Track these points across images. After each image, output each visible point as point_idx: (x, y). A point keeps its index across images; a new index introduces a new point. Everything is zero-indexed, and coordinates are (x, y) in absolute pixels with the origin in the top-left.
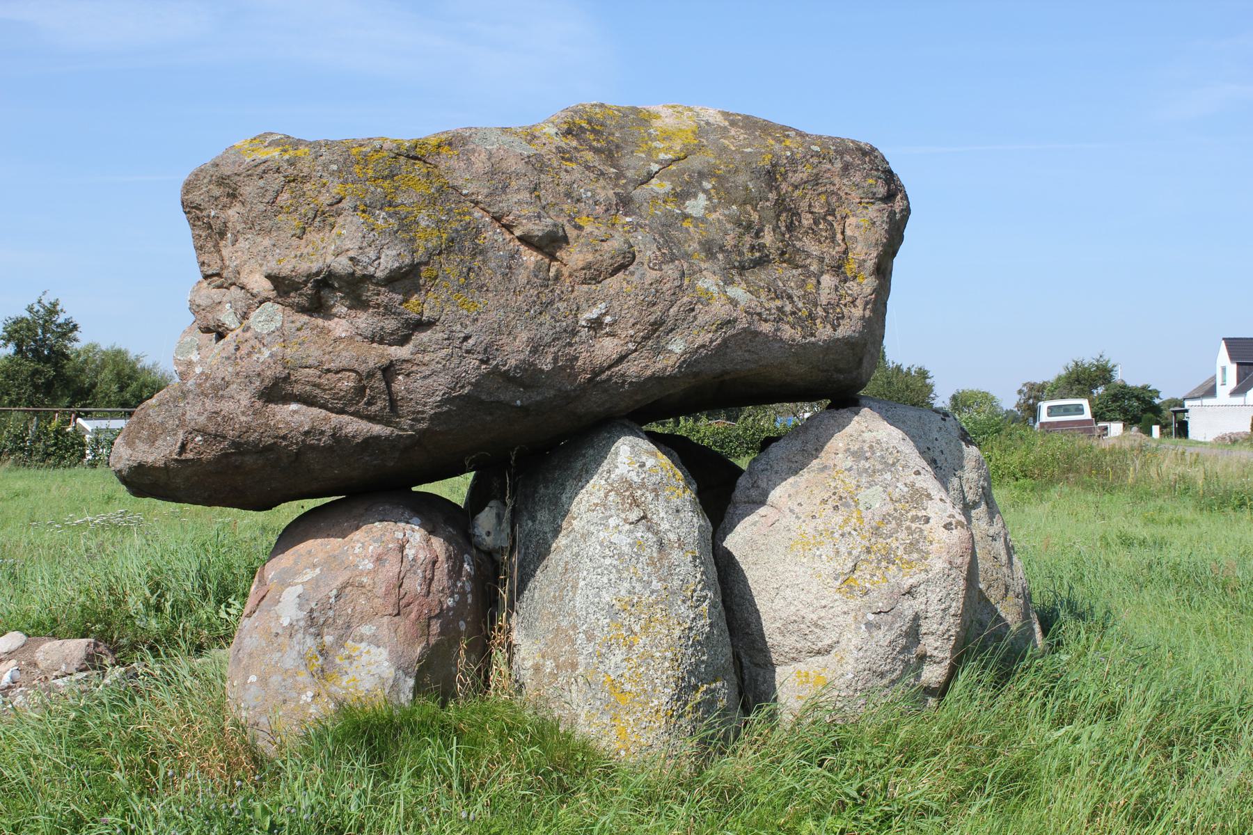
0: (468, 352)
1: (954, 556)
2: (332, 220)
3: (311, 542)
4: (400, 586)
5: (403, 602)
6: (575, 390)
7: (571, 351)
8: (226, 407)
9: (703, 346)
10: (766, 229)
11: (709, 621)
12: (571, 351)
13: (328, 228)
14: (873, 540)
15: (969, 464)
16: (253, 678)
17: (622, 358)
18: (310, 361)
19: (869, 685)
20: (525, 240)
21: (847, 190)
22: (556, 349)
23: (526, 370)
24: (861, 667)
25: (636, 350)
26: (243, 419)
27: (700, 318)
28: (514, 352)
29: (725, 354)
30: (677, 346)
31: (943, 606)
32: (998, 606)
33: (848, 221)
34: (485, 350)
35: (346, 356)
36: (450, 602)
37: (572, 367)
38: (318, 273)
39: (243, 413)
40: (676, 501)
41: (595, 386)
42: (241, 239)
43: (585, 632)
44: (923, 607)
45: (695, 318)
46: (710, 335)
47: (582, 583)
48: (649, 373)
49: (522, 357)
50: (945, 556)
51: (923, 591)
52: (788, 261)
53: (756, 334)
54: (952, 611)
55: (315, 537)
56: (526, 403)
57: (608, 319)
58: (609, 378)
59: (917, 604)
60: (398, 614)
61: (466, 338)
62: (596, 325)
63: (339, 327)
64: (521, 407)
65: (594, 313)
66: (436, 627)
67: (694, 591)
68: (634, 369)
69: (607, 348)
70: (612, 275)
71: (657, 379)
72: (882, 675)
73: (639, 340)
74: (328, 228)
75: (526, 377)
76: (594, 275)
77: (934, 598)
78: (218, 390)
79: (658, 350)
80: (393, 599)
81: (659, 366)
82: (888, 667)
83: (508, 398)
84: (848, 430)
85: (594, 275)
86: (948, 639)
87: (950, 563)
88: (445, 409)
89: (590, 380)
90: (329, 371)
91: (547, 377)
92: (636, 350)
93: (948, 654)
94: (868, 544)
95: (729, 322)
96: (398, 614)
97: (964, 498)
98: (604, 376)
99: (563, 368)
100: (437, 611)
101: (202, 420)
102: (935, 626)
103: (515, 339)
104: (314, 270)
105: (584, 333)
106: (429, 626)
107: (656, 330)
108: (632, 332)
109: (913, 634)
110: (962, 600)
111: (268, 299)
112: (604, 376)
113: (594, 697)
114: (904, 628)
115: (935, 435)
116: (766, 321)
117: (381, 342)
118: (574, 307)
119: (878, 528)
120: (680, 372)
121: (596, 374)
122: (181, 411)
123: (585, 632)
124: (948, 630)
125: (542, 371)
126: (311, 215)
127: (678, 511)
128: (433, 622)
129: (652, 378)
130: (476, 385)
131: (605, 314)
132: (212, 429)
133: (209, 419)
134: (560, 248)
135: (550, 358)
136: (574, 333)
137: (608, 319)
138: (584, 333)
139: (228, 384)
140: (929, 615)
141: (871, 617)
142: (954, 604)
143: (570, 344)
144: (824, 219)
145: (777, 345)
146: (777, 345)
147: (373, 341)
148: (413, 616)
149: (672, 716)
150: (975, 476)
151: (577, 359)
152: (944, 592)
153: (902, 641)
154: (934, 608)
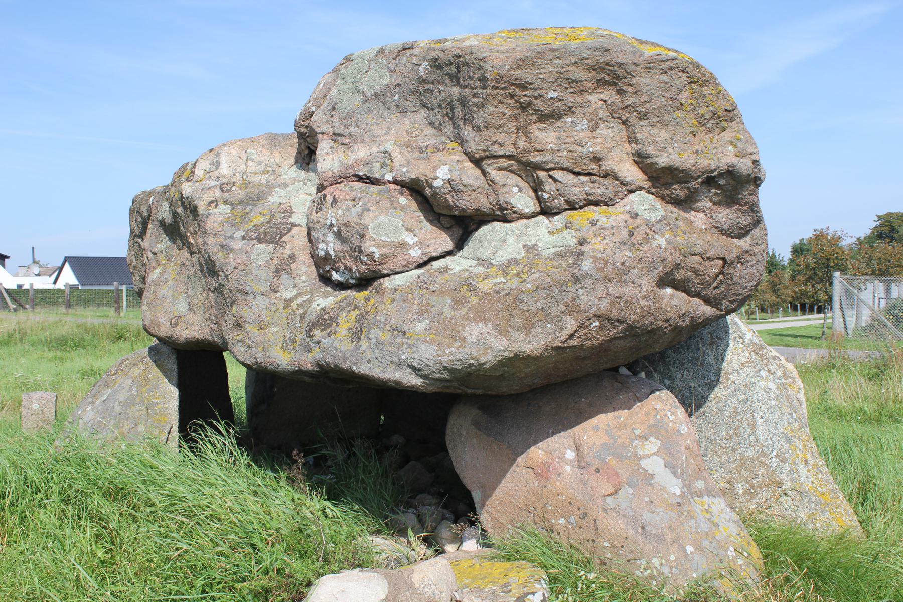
2: (725, 124)
3: (602, 417)
8: (628, 291)
13: (718, 131)
16: (690, 549)
18: (697, 250)
26: (644, 303)
35: (699, 243)
38: (712, 171)
39: (644, 298)
42: (602, 126)
43: (777, 456)
47: (760, 421)
55: (605, 412)
63: (699, 220)
74: (718, 131)
78: (622, 274)
90: (708, 258)
101: (604, 305)
104: (713, 167)
111: (641, 188)
113: (808, 502)
117: (729, 236)
122: (570, 297)
123: (777, 456)
126: (708, 116)
132: (614, 314)
133: (612, 304)
139: (629, 269)
147: (723, 234)
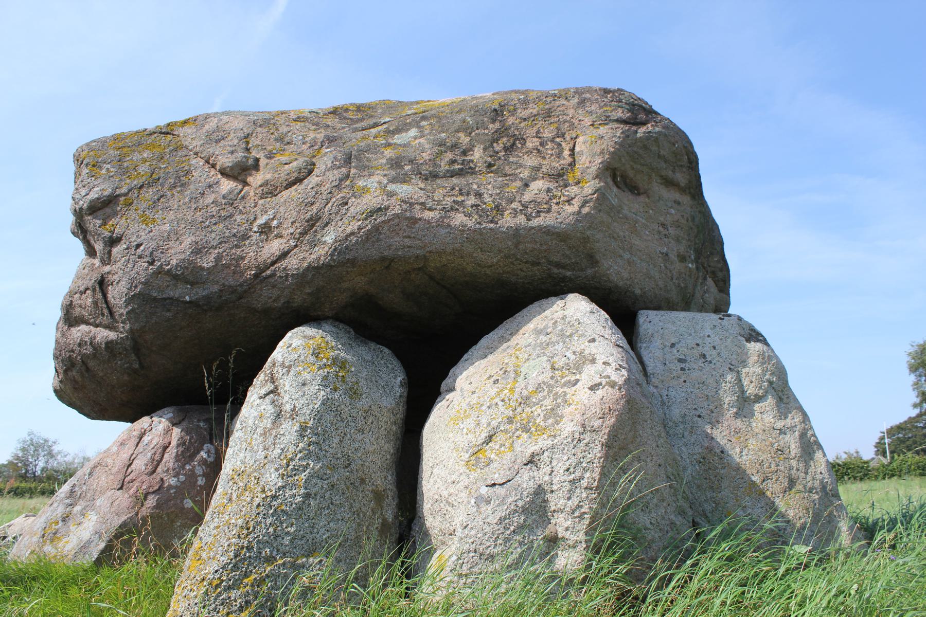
0: (140, 257)
1: (590, 419)
4: (130, 465)
5: (128, 479)
6: (241, 285)
7: (238, 252)
9: (352, 233)
10: (476, 149)
11: (302, 491)
12: (238, 252)
14: (519, 410)
15: (753, 358)
17: (284, 255)
19: (476, 569)
20: (224, 173)
21: (581, 118)
22: (221, 250)
23: (187, 268)
24: (466, 547)
25: (296, 246)
27: (352, 210)
28: (177, 254)
29: (378, 240)
30: (329, 237)
31: (571, 477)
32: (777, 501)
33: (578, 140)
34: (152, 253)
36: (173, 481)
37: (238, 265)
40: (306, 376)
41: (262, 281)
44: (547, 478)
45: (348, 210)
46: (360, 223)
48: (305, 265)
49: (183, 257)
50: (578, 418)
51: (547, 460)
52: (497, 172)
53: (414, 221)
54: (584, 483)
56: (194, 299)
57: (275, 223)
58: (273, 275)
59: (541, 475)
60: (121, 488)
61: (138, 246)
62: (266, 229)
64: (190, 302)
65: (261, 221)
66: (151, 501)
67: (291, 459)
68: (293, 263)
69: (275, 247)
70: (286, 188)
71: (315, 270)
72: (492, 558)
73: (297, 236)
75: (187, 274)
76: (270, 190)
77: (560, 467)
79: (314, 244)
80: (120, 477)
81: (314, 256)
82: (499, 549)
83: (177, 295)
84: (547, 313)
85: (270, 190)
86: (581, 517)
87: (583, 426)
88: (130, 308)
89: (256, 276)
91: (209, 273)
92: (296, 246)
93: (582, 536)
94: (511, 414)
95: (380, 209)
96: (121, 488)
97: (743, 392)
98: (268, 272)
99: (227, 266)
100: (156, 488)
102: (562, 501)
103: (181, 243)
105: (255, 237)
106: (145, 498)
107: (313, 225)
108: (292, 230)
109: (537, 508)
110: (598, 470)
112: (268, 272)
114: (520, 504)
115: (708, 331)
116: (430, 209)
118: (252, 218)
119: (528, 398)
120: (332, 259)
121: (261, 269)
124: (579, 506)
125: (202, 269)
127: (304, 385)
128: (150, 497)
129: (309, 267)
130: (146, 284)
131: (273, 219)
134: (251, 175)
135: (212, 258)
136: (245, 237)
137: (275, 223)
138: (255, 237)
140: (555, 488)
141: (484, 490)
142: (588, 475)
143: (237, 246)
144: (552, 141)
145: (443, 232)
146: (443, 232)
148: (131, 492)
149: (217, 586)
150: (758, 370)
151: (243, 258)
152: (573, 461)
153: (518, 519)
154: (560, 479)
